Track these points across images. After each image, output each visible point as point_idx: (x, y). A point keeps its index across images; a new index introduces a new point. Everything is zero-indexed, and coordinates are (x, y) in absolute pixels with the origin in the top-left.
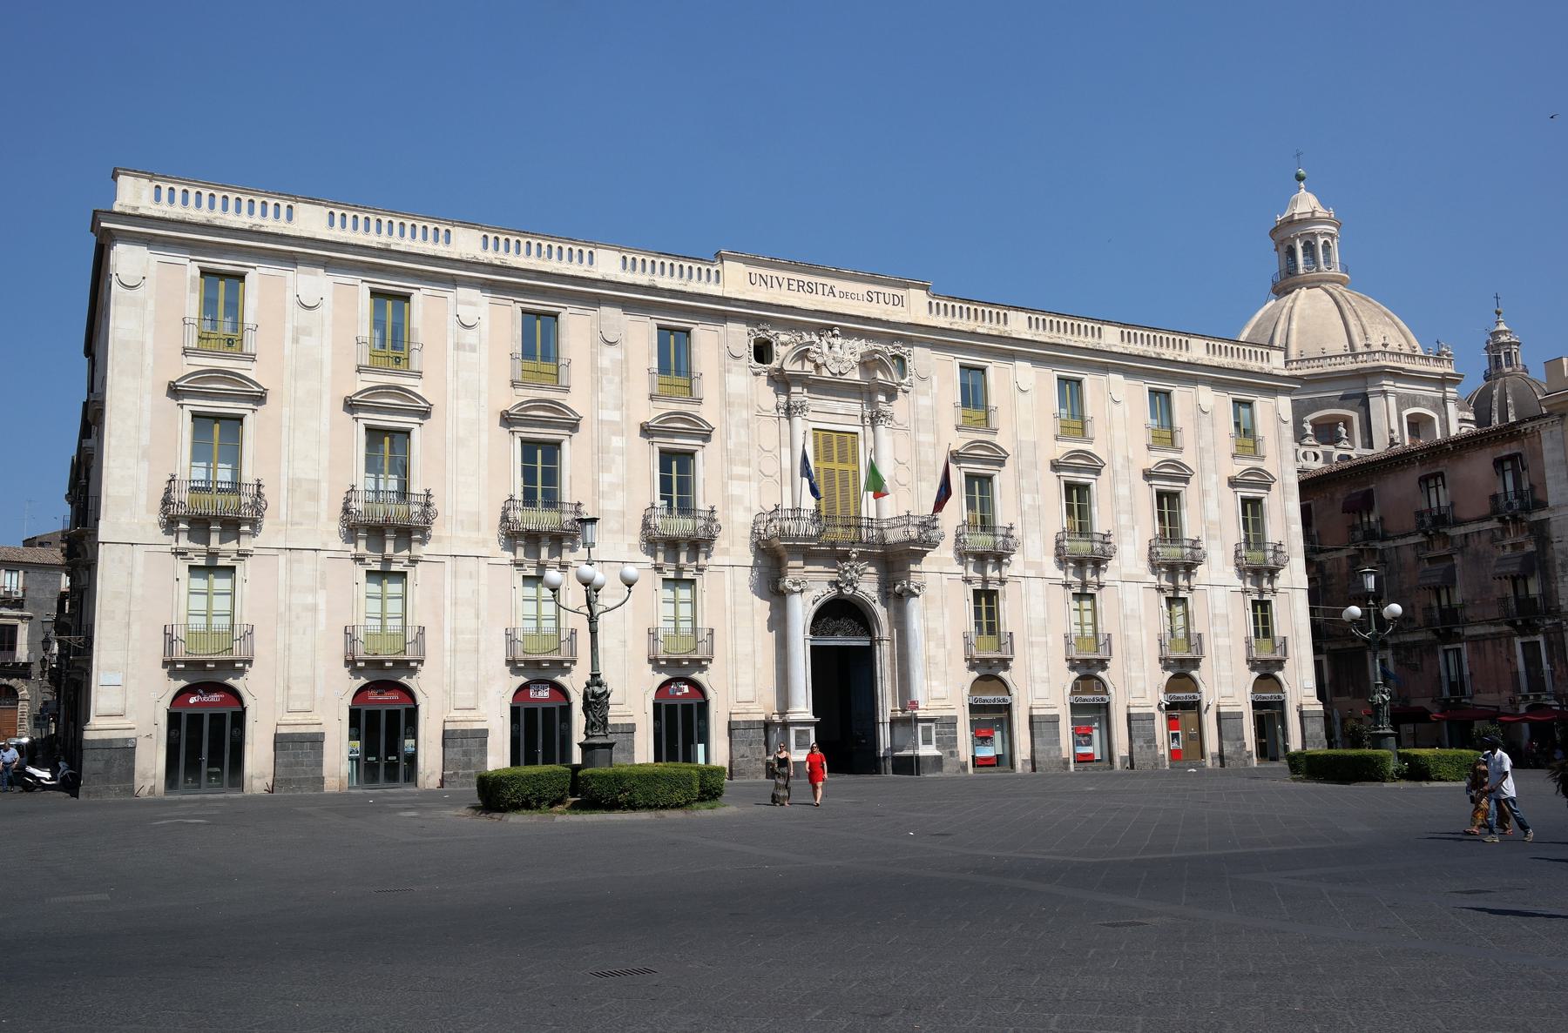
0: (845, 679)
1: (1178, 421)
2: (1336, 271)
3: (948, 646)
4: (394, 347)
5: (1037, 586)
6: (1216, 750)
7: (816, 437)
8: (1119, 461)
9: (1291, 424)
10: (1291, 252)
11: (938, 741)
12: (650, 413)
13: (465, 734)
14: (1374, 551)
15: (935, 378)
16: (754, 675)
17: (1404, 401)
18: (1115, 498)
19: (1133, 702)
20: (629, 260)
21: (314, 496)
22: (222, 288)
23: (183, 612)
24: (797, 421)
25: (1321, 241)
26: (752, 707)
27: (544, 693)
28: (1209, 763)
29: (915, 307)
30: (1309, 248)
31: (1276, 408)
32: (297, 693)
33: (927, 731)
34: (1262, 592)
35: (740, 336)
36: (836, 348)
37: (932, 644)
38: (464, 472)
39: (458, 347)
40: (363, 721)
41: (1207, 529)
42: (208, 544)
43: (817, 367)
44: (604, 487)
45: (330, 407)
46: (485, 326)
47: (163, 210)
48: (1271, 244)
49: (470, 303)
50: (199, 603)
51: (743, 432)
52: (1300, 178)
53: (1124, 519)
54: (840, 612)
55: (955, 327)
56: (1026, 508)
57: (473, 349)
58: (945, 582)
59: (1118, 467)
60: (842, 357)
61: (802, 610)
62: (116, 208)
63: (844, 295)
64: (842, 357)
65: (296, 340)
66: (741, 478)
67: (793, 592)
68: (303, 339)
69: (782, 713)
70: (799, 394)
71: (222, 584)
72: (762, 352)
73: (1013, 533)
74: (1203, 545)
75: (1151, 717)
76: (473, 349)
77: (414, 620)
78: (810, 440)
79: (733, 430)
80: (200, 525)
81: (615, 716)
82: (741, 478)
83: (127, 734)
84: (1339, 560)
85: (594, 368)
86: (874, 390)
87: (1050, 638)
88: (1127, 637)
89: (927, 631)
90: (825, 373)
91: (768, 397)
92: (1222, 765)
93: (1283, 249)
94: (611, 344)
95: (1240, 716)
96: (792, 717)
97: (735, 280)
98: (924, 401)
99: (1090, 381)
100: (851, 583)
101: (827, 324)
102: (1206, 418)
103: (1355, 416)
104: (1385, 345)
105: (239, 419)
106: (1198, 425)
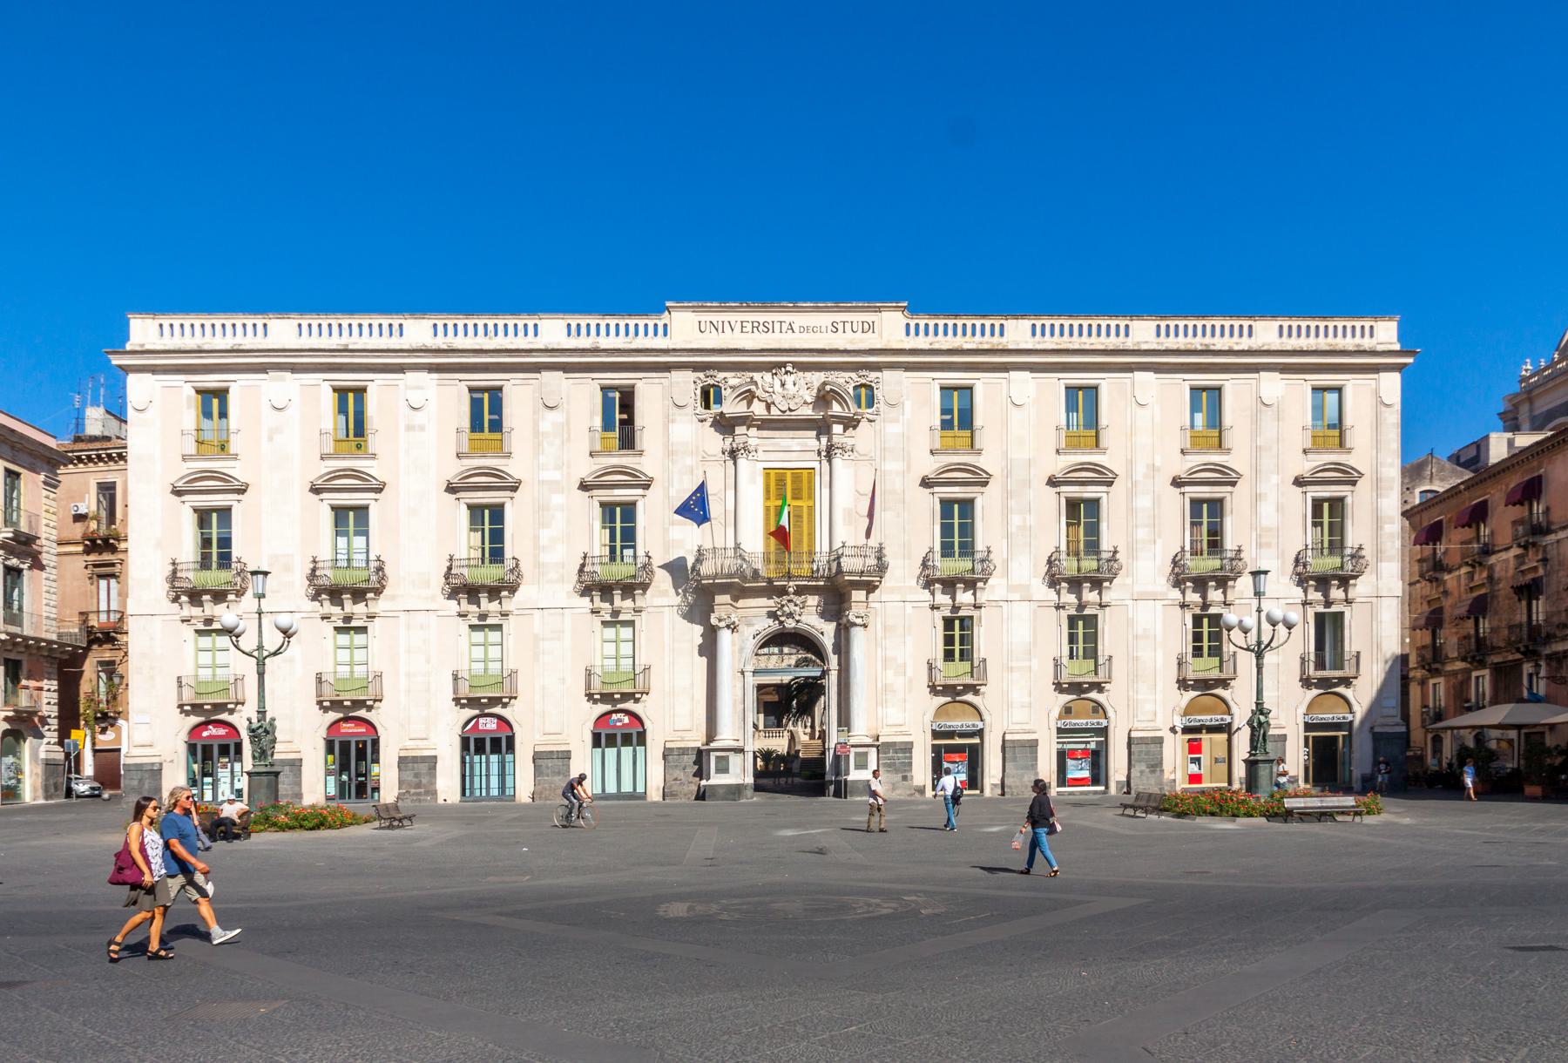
3: (909, 674)
4: (356, 435)
5: (1022, 611)
8: (1140, 471)
9: (1398, 407)
18: (1131, 511)
20: (574, 327)
22: (214, 401)
23: (466, 661)
24: (741, 462)
26: (687, 735)
27: (213, 731)
29: (890, 327)
32: (419, 723)
34: (1328, 604)
35: (686, 384)
36: (789, 385)
37: (890, 673)
38: (420, 534)
39: (409, 428)
40: (473, 744)
42: (612, 603)
43: (768, 407)
44: (544, 541)
47: (168, 343)
50: (478, 653)
55: (936, 346)
56: (1013, 529)
57: (422, 428)
60: (796, 393)
62: (128, 347)
65: (270, 439)
67: (855, 625)
70: (753, 437)
71: (494, 636)
72: (708, 396)
73: (1363, 553)
75: (1159, 741)
76: (422, 428)
77: (642, 661)
80: (335, 594)
81: (281, 752)
83: (156, 760)
84: (1507, 561)
85: (536, 432)
87: (1035, 663)
90: (774, 411)
91: (716, 442)
94: (892, 405)
97: (686, 327)
98: (893, 429)
99: (1108, 385)
100: (790, 615)
101: (775, 363)
102: (1268, 415)
106: (1256, 420)
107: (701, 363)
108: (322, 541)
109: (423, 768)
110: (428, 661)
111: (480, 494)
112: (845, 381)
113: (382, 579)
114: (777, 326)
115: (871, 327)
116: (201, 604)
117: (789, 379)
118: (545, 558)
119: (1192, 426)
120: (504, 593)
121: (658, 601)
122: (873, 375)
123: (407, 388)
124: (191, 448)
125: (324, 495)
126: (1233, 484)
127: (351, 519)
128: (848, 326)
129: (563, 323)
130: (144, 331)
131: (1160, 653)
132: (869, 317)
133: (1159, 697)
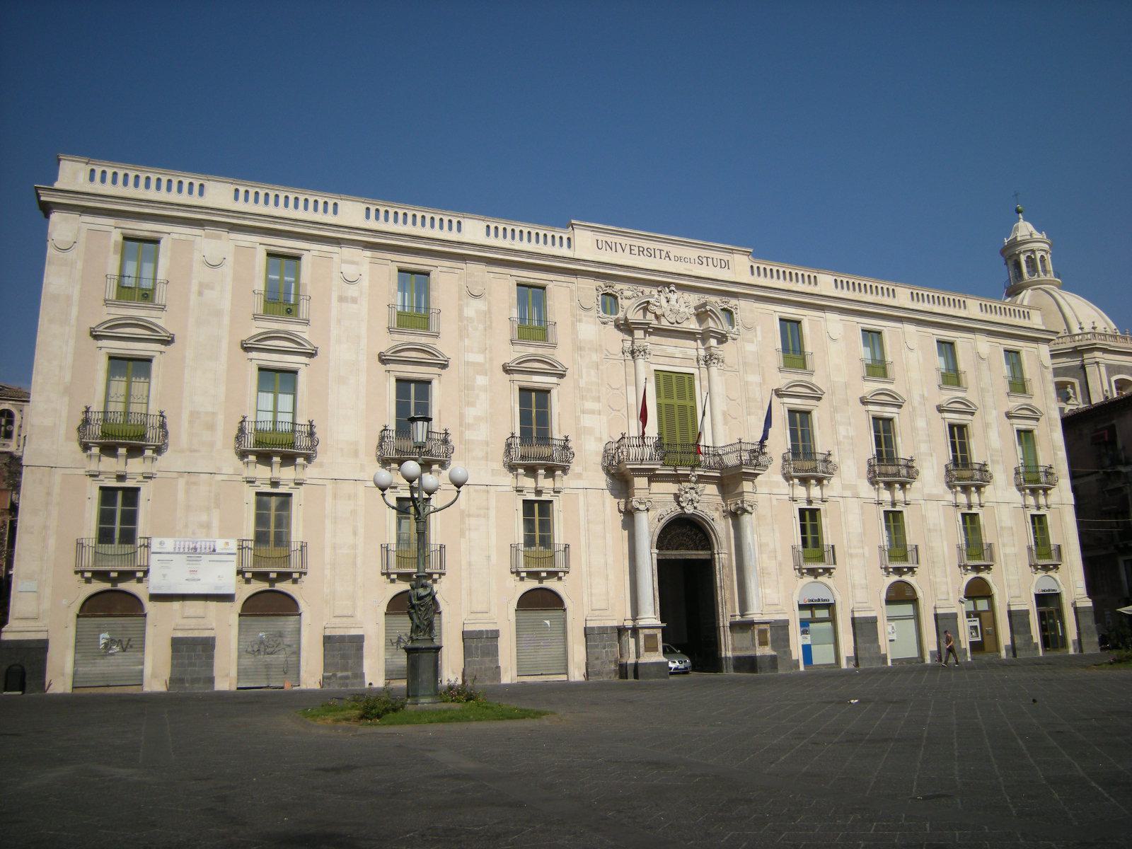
0: (688, 578)
1: (962, 366)
2: (1051, 276)
3: (779, 558)
6: (1009, 643)
7: (657, 377)
10: (1017, 265)
11: (773, 642)
12: (512, 354)
13: (342, 639)
14: (1119, 472)
15: (758, 329)
16: (608, 582)
17: (1112, 369)
19: (939, 603)
21: (211, 427)
24: (640, 362)
25: (1038, 255)
28: (1003, 654)
29: (739, 267)
30: (1031, 262)
31: (1038, 356)
33: (763, 632)
35: (589, 289)
36: (673, 302)
37: (765, 556)
39: (342, 299)
41: (992, 455)
43: (657, 317)
44: (469, 420)
45: (227, 347)
46: (365, 282)
48: (1002, 260)
49: (353, 263)
51: (593, 372)
52: (1018, 212)
53: (924, 448)
54: (685, 531)
57: (354, 301)
58: (775, 502)
59: (916, 403)
60: (680, 308)
61: (648, 526)
62: (57, 185)
63: (679, 259)
64: (680, 308)
65: (200, 294)
66: (592, 412)
68: (206, 292)
69: (635, 618)
72: (610, 301)
74: (989, 468)
76: (354, 301)
78: (653, 379)
79: (584, 370)
82: (592, 412)
86: (710, 333)
88: (931, 548)
89: (761, 546)
92: (1015, 655)
93: (1011, 263)
95: (1027, 612)
96: (641, 623)
97: (586, 243)
98: (750, 348)
102: (984, 366)
103: (1076, 382)
104: (1094, 328)
105: (148, 360)
107: (606, 276)
108: (96, 389)
109: (474, 643)
110: (355, 533)
111: (410, 368)
112: (715, 302)
113: (313, 446)
114: (658, 253)
115: (727, 264)
116: (553, 477)
117: (673, 297)
118: (469, 435)
119: (122, 276)
120: (559, 473)
121: (574, 484)
122: (733, 302)
123: (343, 261)
124: (112, 295)
125: (254, 355)
126: (819, 399)
127: (278, 379)
128: (710, 260)
129: (233, 187)
130: (73, 175)
131: (945, 543)
132: (726, 257)
133: (949, 580)
